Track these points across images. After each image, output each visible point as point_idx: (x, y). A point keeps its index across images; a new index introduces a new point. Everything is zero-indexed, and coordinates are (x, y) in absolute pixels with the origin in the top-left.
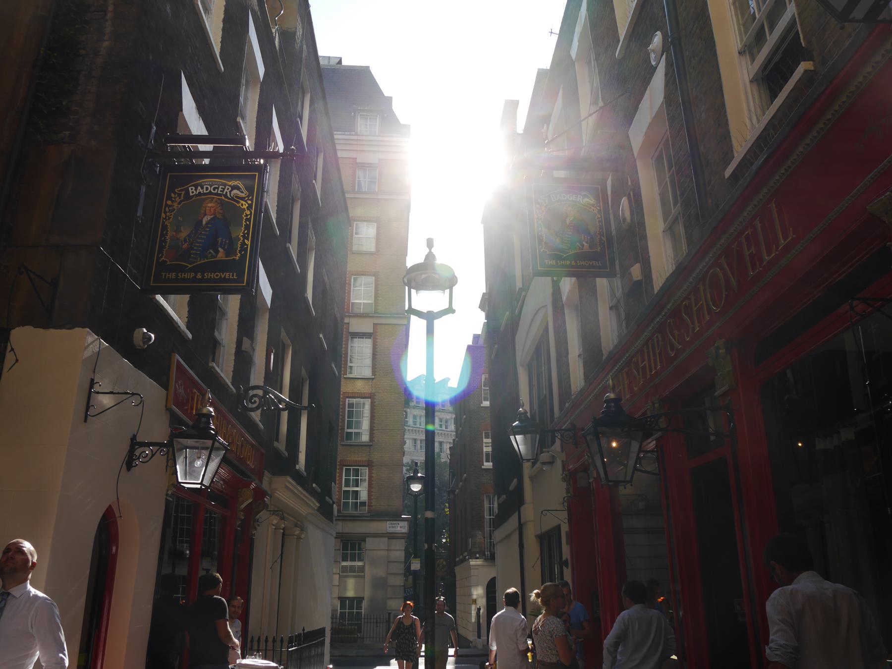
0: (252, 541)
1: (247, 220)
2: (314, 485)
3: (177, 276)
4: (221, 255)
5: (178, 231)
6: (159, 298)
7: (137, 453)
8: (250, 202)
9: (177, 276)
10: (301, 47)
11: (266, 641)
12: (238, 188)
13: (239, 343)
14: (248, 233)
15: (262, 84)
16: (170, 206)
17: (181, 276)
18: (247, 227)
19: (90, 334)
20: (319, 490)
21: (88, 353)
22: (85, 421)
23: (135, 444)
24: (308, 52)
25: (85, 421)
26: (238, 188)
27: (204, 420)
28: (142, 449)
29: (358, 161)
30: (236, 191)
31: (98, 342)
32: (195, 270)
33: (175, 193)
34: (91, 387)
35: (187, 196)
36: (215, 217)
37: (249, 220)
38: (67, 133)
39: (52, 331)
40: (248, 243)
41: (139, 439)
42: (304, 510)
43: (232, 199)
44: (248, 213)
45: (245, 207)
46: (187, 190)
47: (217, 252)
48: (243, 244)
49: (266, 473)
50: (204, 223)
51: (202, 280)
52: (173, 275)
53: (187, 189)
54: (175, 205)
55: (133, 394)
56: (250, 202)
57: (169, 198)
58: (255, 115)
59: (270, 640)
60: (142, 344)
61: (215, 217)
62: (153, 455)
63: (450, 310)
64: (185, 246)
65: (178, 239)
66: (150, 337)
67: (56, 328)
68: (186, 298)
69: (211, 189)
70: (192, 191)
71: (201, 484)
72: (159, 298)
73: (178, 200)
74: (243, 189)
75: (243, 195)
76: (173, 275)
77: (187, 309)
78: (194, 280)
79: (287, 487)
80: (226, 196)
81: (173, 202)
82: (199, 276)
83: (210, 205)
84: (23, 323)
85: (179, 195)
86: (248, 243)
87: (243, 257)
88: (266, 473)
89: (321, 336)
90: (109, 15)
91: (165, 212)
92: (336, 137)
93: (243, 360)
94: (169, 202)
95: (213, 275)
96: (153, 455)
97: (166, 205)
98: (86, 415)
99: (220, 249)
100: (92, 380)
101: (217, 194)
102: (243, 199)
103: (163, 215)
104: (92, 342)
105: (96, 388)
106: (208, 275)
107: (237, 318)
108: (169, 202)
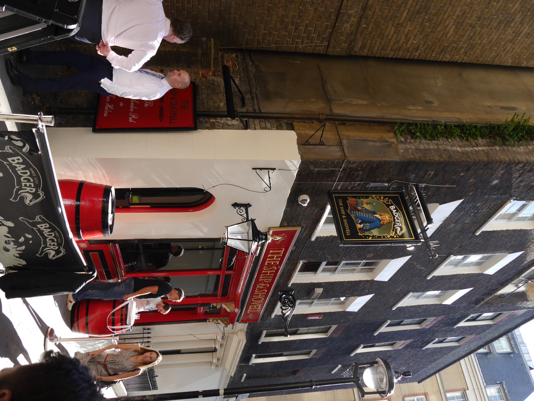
0: (205, 320)
1: (384, 236)
3: (341, 206)
4: (359, 226)
5: (367, 204)
6: (329, 208)
8: (395, 237)
9: (341, 206)
10: (521, 308)
11: (149, 337)
12: (401, 230)
14: (376, 238)
15: (482, 275)
16: (380, 198)
17: (342, 209)
18: (379, 237)
21: (288, 163)
22: (253, 169)
23: (247, 206)
24: (521, 316)
25: (253, 169)
26: (401, 230)
29: (467, 391)
30: (399, 229)
32: (347, 214)
33: (388, 200)
34: (271, 169)
35: (388, 206)
36: (381, 221)
37: (384, 237)
38: (403, 140)
39: (296, 146)
40: (370, 238)
41: (249, 209)
42: (228, 365)
43: (394, 228)
44: (389, 237)
45: (391, 235)
46: (392, 205)
47: (360, 224)
48: (369, 236)
49: (247, 325)
50: (376, 215)
51: (342, 219)
52: (341, 204)
54: (382, 201)
55: (270, 188)
56: (395, 237)
57: (385, 197)
59: (149, 331)
60: (300, 200)
61: (381, 221)
62: (241, 215)
63: (363, 393)
64: (359, 208)
65: (362, 204)
66: (304, 203)
67: (298, 147)
68: (335, 234)
69: (396, 216)
70: (392, 208)
71: (228, 238)
72: (329, 208)
74: (402, 233)
75: (398, 232)
76: (341, 204)
77: (328, 235)
78: (341, 215)
79: (240, 341)
80: (395, 224)
81: (383, 199)
82: (344, 217)
83: (387, 217)
85: (388, 202)
86: (370, 238)
87: (361, 237)
89: (340, 366)
90: (476, 148)
91: (376, 196)
92: (472, 355)
94: (382, 198)
95: (346, 223)
96: (241, 215)
97: (380, 197)
98: (256, 169)
99: (362, 225)
100: (275, 169)
102: (396, 233)
103: (374, 196)
104: (294, 164)
105: (271, 171)
107: (333, 281)
108: (382, 198)
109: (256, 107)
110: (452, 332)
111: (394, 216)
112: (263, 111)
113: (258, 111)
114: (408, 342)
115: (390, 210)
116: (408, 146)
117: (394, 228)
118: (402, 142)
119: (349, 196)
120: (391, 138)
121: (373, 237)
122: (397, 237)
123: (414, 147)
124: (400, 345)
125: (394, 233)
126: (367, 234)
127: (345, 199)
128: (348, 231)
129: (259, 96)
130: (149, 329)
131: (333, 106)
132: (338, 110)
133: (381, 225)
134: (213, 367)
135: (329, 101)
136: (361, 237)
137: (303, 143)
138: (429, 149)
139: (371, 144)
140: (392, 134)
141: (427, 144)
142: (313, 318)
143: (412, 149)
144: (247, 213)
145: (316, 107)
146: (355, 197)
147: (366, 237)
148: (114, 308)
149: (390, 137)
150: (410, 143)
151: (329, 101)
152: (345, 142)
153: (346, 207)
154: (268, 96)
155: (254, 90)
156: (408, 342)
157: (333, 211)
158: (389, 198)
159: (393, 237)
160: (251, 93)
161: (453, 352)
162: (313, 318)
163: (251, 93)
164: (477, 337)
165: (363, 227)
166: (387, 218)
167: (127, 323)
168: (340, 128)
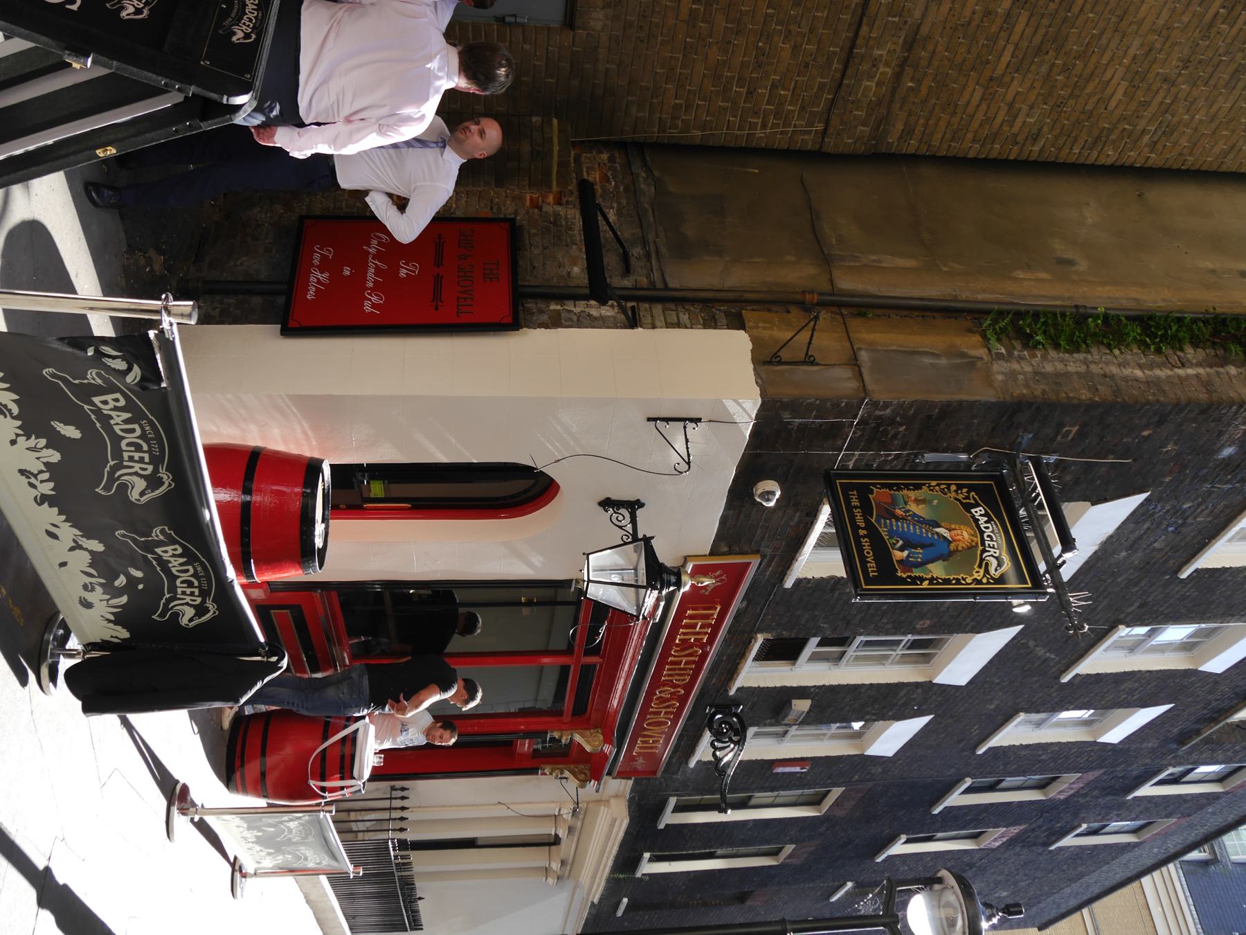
0: (532, 771)
2: (625, 900)
3: (856, 507)
4: (898, 555)
5: (918, 501)
6: (826, 512)
7: (623, 511)
8: (985, 581)
9: (856, 507)
12: (1000, 565)
13: (801, 692)
14: (938, 583)
15: (1195, 672)
16: (949, 488)
17: (858, 513)
18: (947, 581)
19: (755, 404)
20: (620, 913)
21: (731, 406)
22: (649, 419)
23: (634, 506)
25: (649, 419)
26: (1000, 565)
27: (673, 579)
28: (627, 515)
30: (994, 563)
31: (746, 419)
32: (870, 527)
34: (691, 420)
35: (968, 507)
36: (950, 542)
40: (925, 585)
41: (639, 512)
42: (585, 876)
43: (982, 560)
44: (969, 580)
45: (976, 576)
46: (977, 505)
47: (901, 549)
48: (922, 580)
49: (631, 782)
50: (938, 530)
52: (855, 502)
53: (979, 505)
54: (953, 495)
55: (689, 463)
56: (985, 581)
57: (960, 487)
58: (1143, 668)
60: (759, 492)
61: (950, 542)
62: (620, 527)
64: (899, 512)
65: (906, 503)
66: (768, 500)
67: (755, 369)
69: (988, 532)
70: (978, 511)
71: (589, 581)
72: (826, 512)
73: (960, 497)
74: (1000, 571)
75: (992, 571)
76: (855, 502)
78: (856, 528)
79: (614, 820)
80: (984, 551)
82: (862, 532)
83: (965, 534)
84: (754, 340)
85: (968, 498)
86: (925, 585)
87: (903, 581)
88: (631, 782)
89: (850, 885)
90: (1181, 372)
91: (938, 485)
92: (1171, 866)
93: (773, 707)
94: (953, 488)
96: (620, 527)
97: (949, 486)
98: (655, 419)
100: (699, 420)
101: (983, 543)
102: (987, 571)
103: (934, 483)
104: (744, 409)
105: (690, 425)
106: (865, 542)
107: (835, 682)
108: (953, 488)
109: (656, 275)
110: (1123, 810)
111: (982, 533)
112: (671, 285)
113: (659, 285)
114: (1014, 830)
115: (973, 517)
116: (1015, 366)
117: (982, 560)
118: (1000, 356)
119: (874, 485)
120: (974, 347)
121: (931, 580)
122: (988, 583)
123: (1028, 369)
124: (995, 837)
125: (982, 571)
126: (917, 573)
127: (864, 491)
128: (872, 566)
129: (663, 250)
130: (403, 789)
131: (836, 273)
132: (847, 283)
133: (951, 553)
134: (550, 880)
135: (826, 260)
136: (903, 581)
137: (766, 360)
138: (1067, 374)
139: (927, 360)
140: (977, 339)
141: (1062, 361)
142: (787, 770)
143: (1024, 373)
144: (634, 521)
145: (797, 274)
146: (890, 486)
147: (915, 580)
148: (326, 738)
149: (972, 345)
150: (1021, 358)
151: (826, 260)
152: (864, 356)
153: (866, 508)
154: (684, 250)
155: (651, 237)
156: (1014, 830)
157: (836, 518)
158: (971, 488)
159: (979, 582)
160: (644, 242)
161: (1125, 858)
162: (787, 770)
163: (644, 242)
164: (1184, 822)
165: (908, 556)
166: (964, 535)
167: (355, 774)
168: (854, 323)
